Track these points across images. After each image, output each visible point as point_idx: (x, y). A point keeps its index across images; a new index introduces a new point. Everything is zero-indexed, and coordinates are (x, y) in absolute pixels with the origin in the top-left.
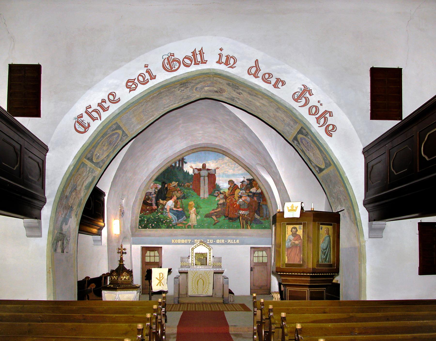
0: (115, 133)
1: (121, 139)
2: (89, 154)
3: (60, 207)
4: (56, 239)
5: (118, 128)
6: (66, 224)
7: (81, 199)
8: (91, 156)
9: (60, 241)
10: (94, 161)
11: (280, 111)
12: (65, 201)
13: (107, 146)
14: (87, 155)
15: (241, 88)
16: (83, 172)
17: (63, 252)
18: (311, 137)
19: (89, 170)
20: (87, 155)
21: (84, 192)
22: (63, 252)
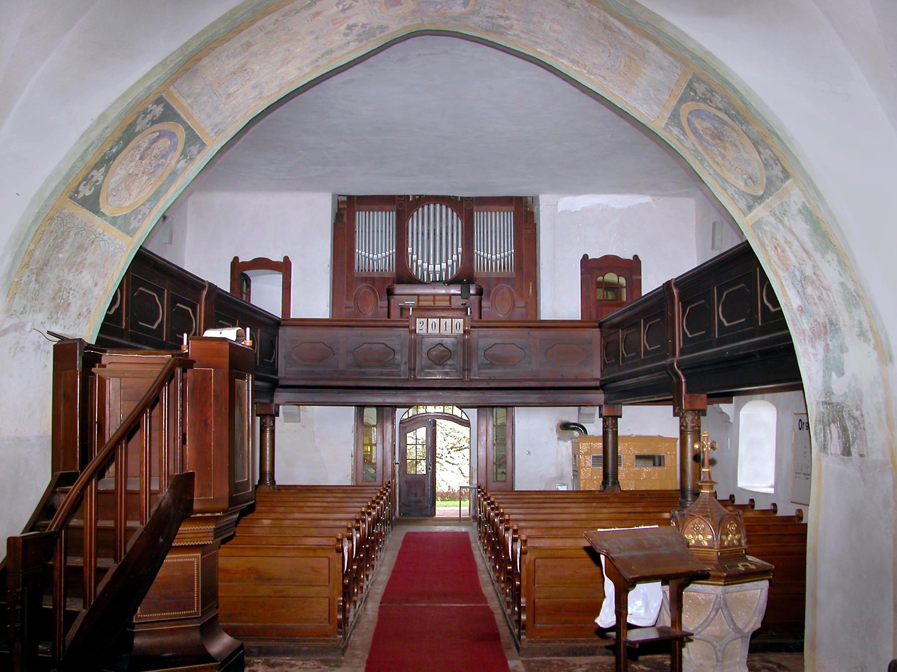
0: (689, 125)
1: (705, 100)
2: (738, 202)
3: (803, 341)
4: (819, 419)
5: (677, 121)
6: (841, 374)
7: (842, 284)
8: (746, 199)
9: (832, 425)
10: (761, 193)
11: (253, 95)
12: (804, 321)
13: (725, 148)
14: (740, 209)
15: (353, 43)
16: (772, 237)
17: (847, 452)
18: (184, 169)
19: (776, 218)
20: (740, 209)
21: (828, 262)
22: (847, 452)
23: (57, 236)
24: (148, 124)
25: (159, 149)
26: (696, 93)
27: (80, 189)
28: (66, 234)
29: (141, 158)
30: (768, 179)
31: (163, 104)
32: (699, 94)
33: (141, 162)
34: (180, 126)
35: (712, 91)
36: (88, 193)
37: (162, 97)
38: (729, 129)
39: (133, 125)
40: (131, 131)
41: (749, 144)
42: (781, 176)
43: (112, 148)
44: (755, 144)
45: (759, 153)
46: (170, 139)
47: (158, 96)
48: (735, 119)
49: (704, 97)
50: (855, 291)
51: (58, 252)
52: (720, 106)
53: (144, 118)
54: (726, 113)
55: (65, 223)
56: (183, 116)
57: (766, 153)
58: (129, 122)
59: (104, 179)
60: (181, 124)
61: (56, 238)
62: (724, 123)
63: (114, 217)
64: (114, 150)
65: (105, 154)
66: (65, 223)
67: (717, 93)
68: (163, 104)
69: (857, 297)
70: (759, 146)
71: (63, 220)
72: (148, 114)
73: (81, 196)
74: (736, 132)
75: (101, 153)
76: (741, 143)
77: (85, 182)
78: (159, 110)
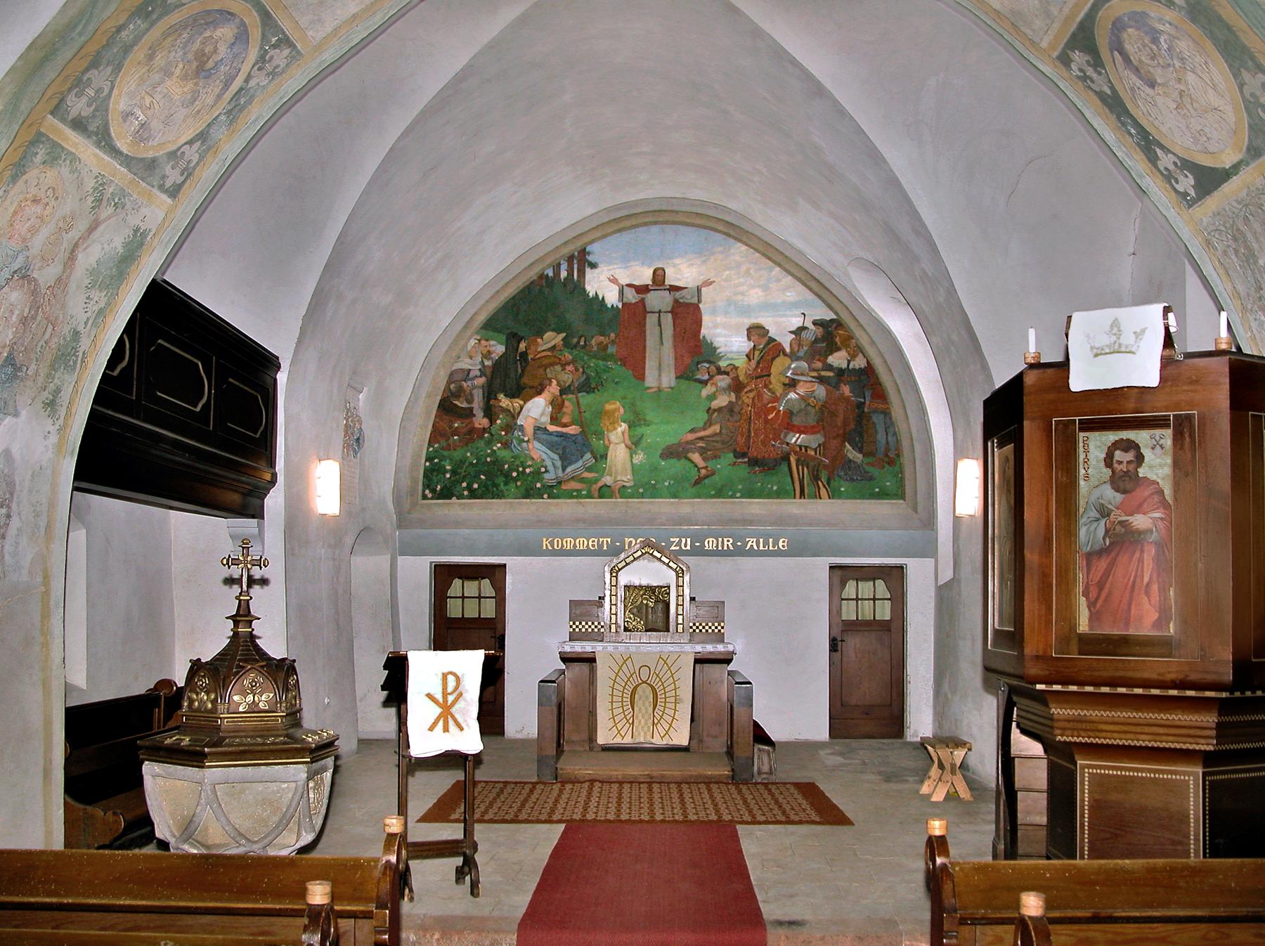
23: (1234, 249)
24: (1100, 74)
25: (1140, 50)
26: (274, 46)
27: (1182, 190)
28: (1238, 236)
29: (1152, 84)
30: (154, 160)
31: (1069, 52)
32: (272, 53)
33: (1160, 84)
34: (1100, 14)
35: (273, 74)
36: (1191, 180)
37: (1058, 58)
38: (217, 91)
39: (1101, 96)
40: (1110, 100)
41: (201, 126)
42: (168, 183)
43: (1130, 134)
44: (202, 136)
45: (190, 143)
46: (1124, 28)
47: (1058, 64)
48: (233, 103)
49: (267, 58)
50: (84, 353)
51: (1256, 262)
52: (252, 83)
53: (1092, 81)
54: (241, 89)
55: (1223, 229)
56: (1082, 15)
57: (192, 153)
58: (1099, 102)
59: (1174, 154)
60: (1097, 13)
61: (1236, 252)
62: (227, 85)
63: (1248, 149)
64: (1133, 131)
65: (1138, 144)
66: (1223, 229)
67: (270, 81)
68: (1069, 52)
69: (79, 361)
70: (200, 142)
71: (1216, 230)
72: (1085, 74)
73: (1192, 193)
74: (216, 102)
75: (1135, 150)
76: (199, 111)
77: (1173, 181)
78: (1078, 58)
